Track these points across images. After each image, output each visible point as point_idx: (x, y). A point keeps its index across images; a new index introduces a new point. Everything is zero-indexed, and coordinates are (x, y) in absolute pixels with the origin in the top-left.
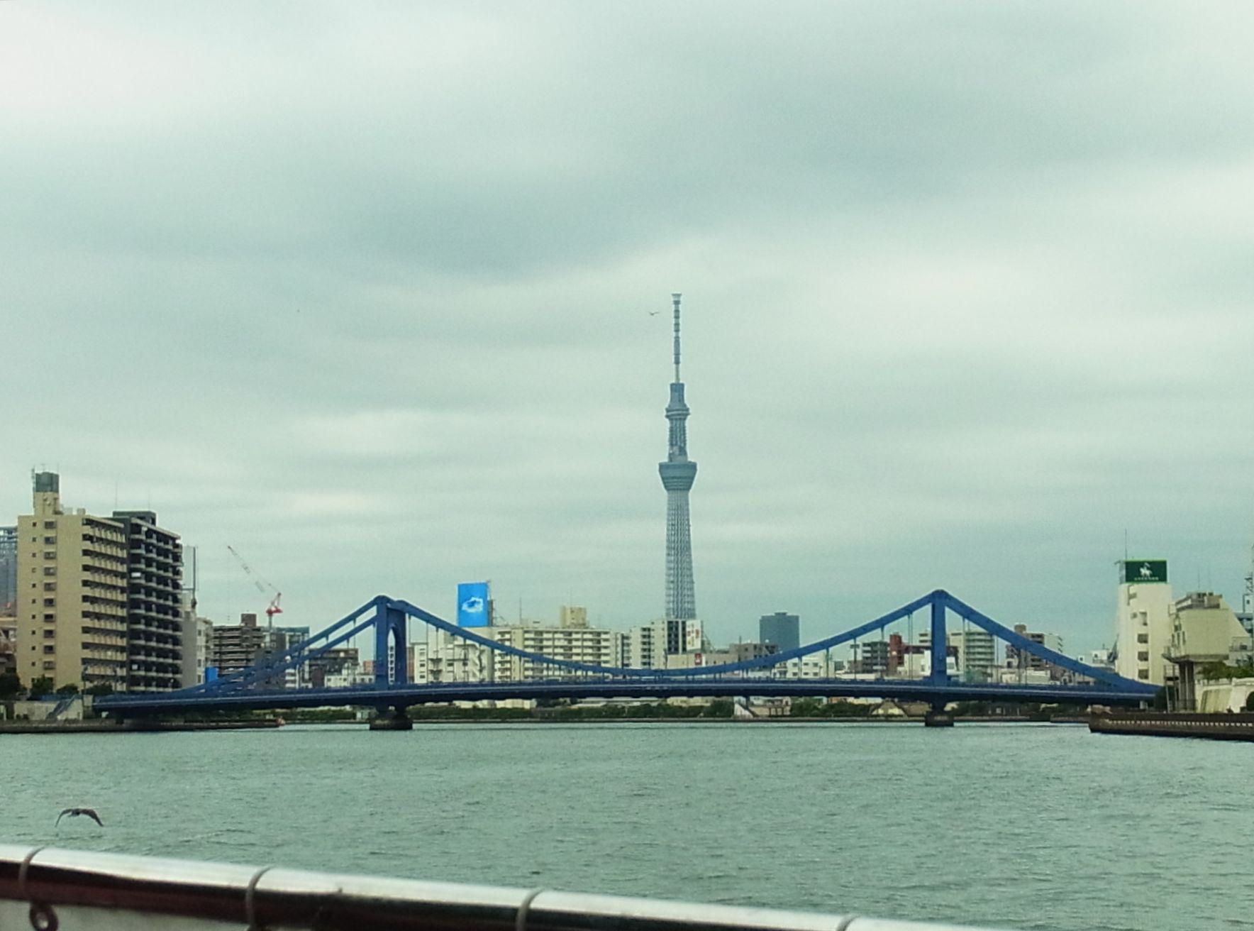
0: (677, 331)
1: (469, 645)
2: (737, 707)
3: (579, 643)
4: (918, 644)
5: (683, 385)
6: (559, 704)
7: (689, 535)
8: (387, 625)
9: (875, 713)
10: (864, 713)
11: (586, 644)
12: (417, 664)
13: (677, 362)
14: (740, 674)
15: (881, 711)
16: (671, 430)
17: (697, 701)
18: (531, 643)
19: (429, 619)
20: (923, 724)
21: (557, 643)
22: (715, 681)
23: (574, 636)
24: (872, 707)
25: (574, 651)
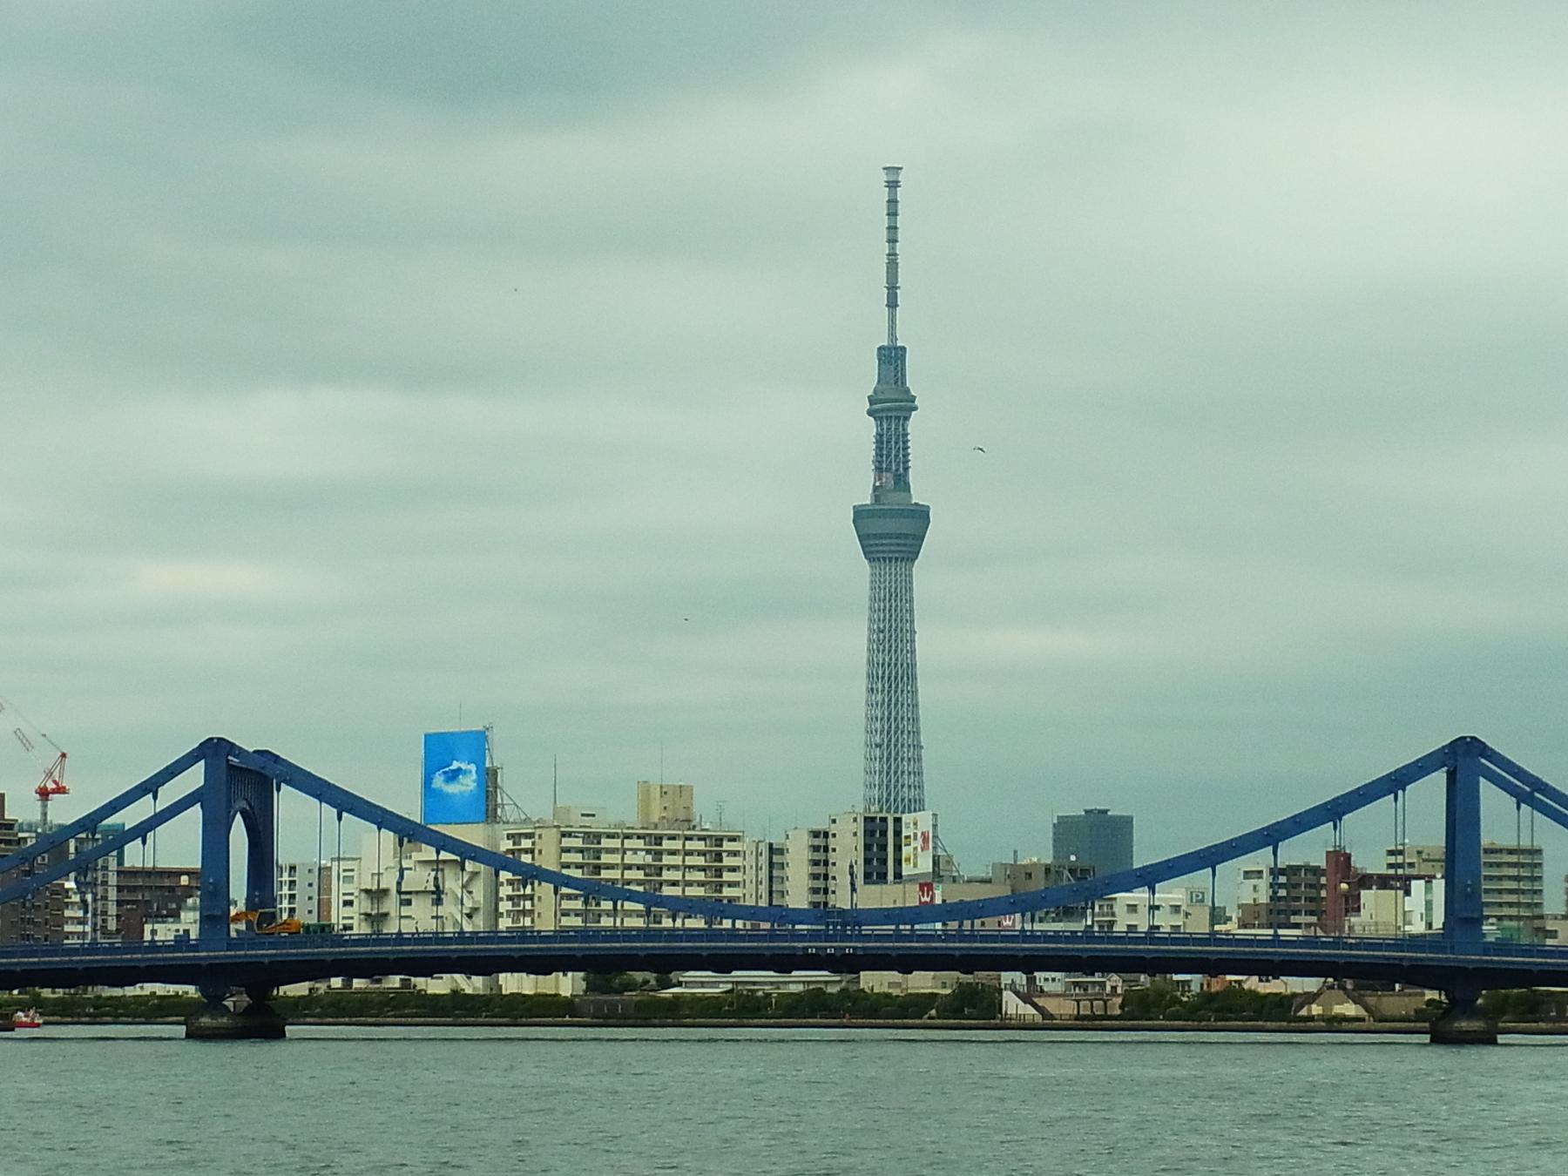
0: (892, 241)
1: (444, 862)
2: (1008, 996)
3: (677, 860)
4: (1383, 871)
5: (903, 349)
6: (631, 986)
7: (913, 652)
8: (229, 806)
9: (1303, 1012)
10: (1280, 1013)
11: (690, 861)
13: (892, 304)
14: (1013, 922)
15: (1316, 1010)
16: (879, 436)
17: (922, 982)
18: (578, 858)
19: (345, 803)
20: (1426, 1038)
21: (630, 859)
22: (960, 936)
23: (666, 844)
24: (1299, 1000)
25: (666, 875)
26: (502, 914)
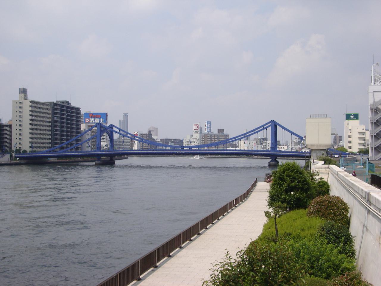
12: (184, 143)
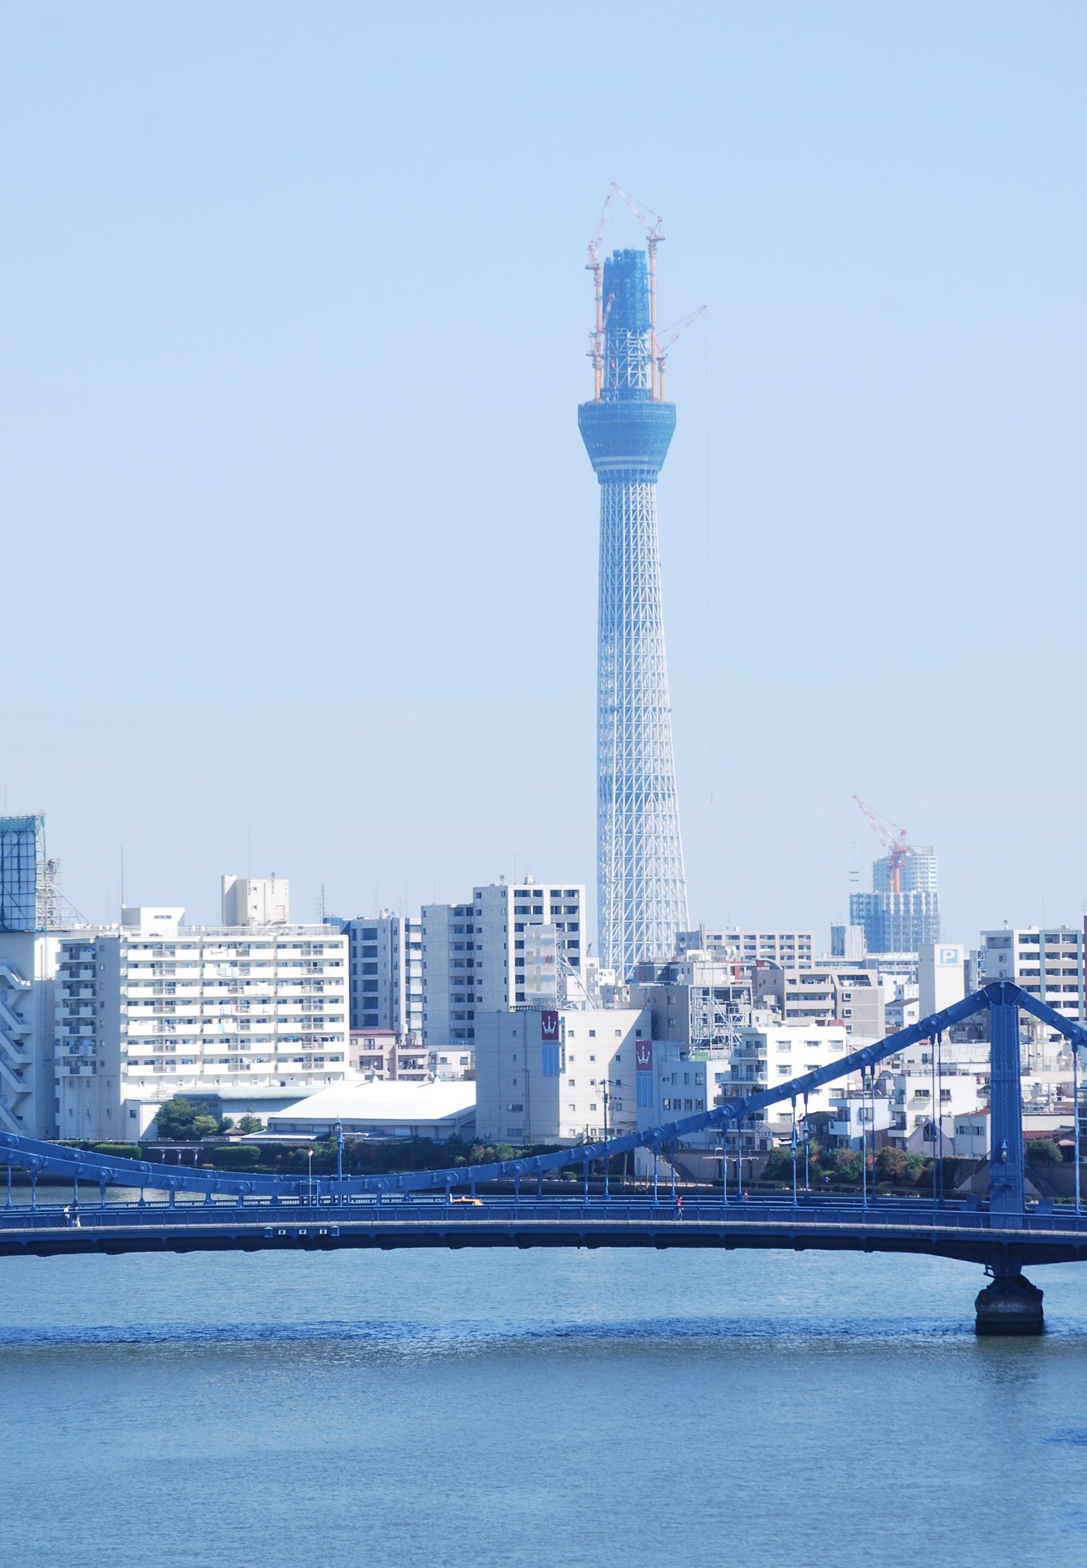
26: (58, 1040)
